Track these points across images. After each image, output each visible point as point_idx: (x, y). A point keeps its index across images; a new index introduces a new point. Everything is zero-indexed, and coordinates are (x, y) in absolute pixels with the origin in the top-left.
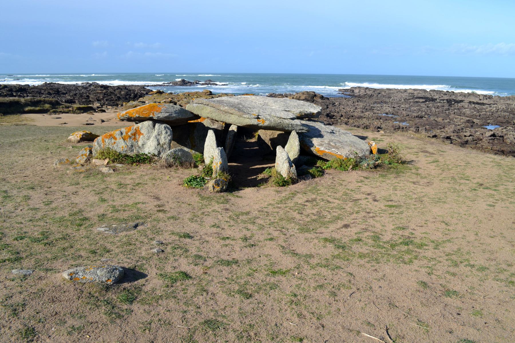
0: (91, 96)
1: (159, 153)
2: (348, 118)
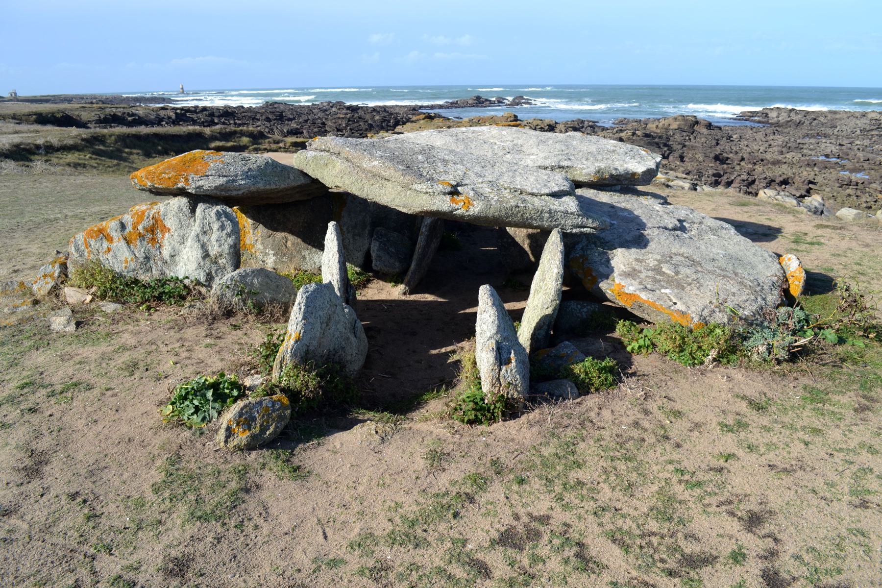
0: (329, 123)
1: (210, 278)
2: (755, 164)
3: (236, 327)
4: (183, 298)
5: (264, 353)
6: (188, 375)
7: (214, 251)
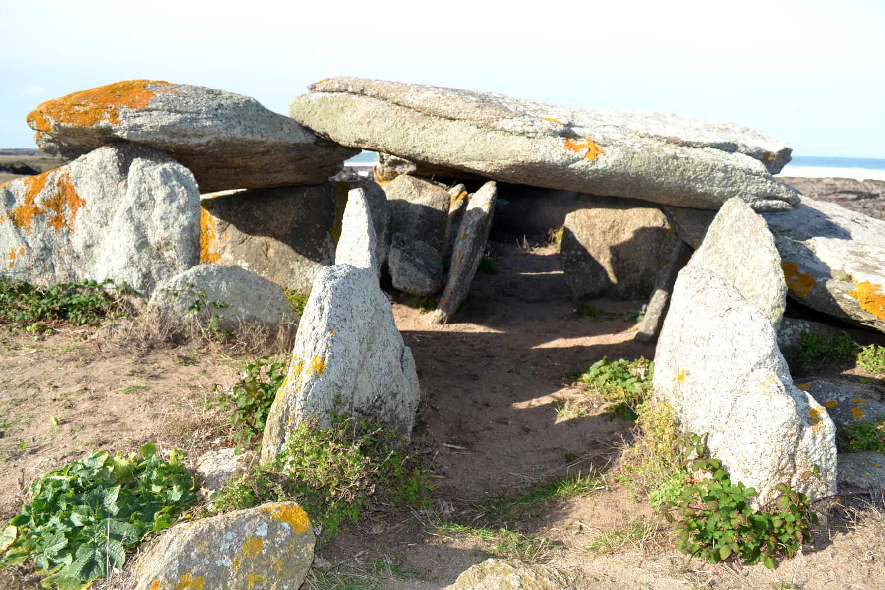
1: (148, 281)
3: (186, 361)
4: (101, 313)
5: (242, 403)
6: (80, 448)
7: (155, 236)
